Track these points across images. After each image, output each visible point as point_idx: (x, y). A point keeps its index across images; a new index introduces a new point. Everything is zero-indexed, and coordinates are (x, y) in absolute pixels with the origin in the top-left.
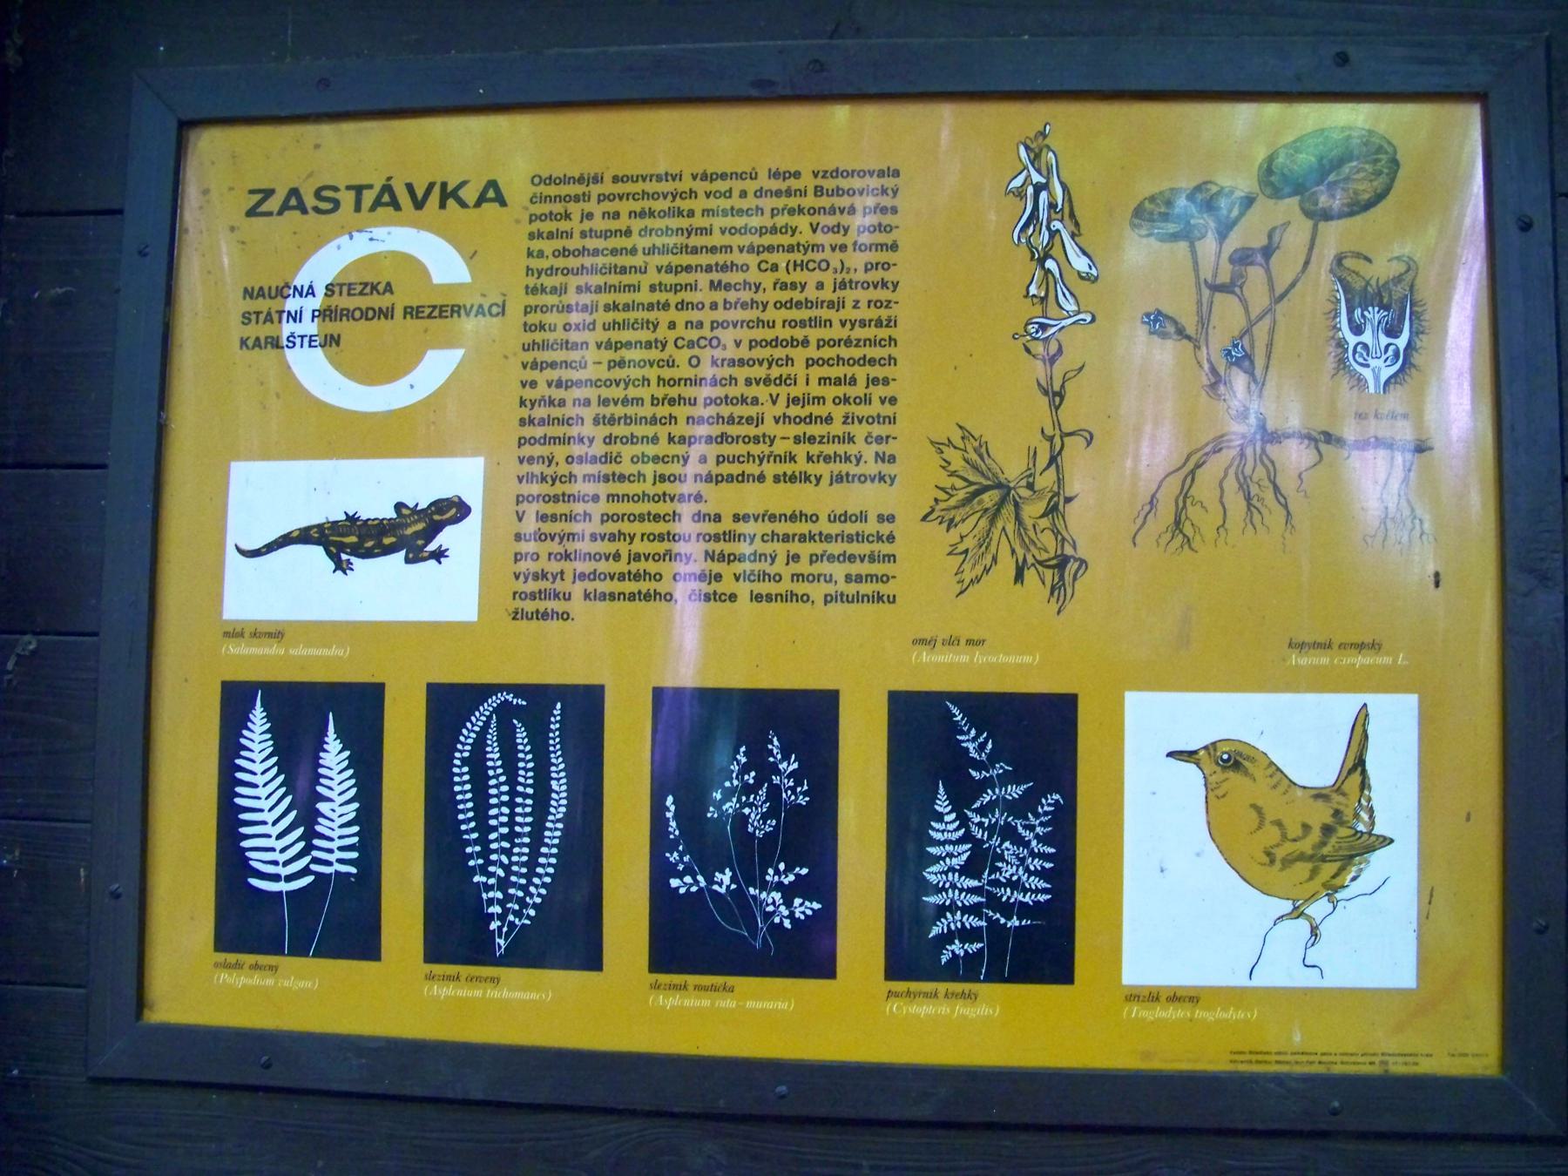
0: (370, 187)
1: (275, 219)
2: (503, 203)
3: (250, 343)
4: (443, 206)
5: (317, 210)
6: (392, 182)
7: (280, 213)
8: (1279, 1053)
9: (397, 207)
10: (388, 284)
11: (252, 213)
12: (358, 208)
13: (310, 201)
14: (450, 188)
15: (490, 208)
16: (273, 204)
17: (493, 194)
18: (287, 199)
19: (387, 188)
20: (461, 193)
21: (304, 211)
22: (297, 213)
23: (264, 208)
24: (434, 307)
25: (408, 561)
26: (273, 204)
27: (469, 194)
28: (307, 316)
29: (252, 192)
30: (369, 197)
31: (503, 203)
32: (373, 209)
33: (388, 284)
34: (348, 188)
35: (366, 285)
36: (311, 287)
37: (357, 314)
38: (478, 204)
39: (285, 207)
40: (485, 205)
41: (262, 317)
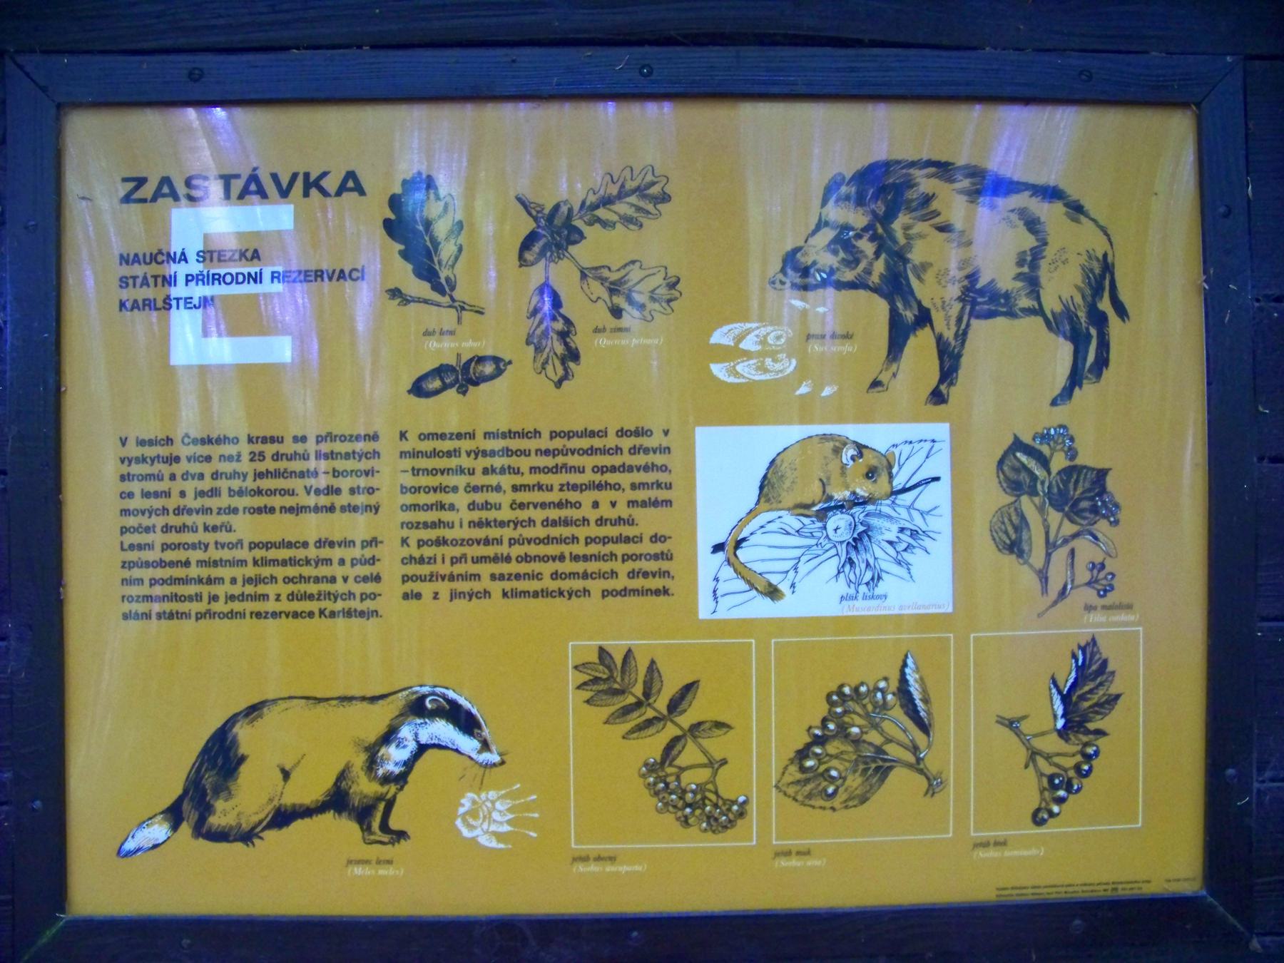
0: (237, 176)
2: (362, 192)
3: (128, 305)
4: (306, 194)
8: (1034, 887)
10: (256, 251)
11: (127, 199)
14: (312, 178)
16: (148, 190)
19: (253, 178)
20: (324, 183)
25: (401, 252)
27: (331, 184)
28: (181, 280)
29: (125, 180)
30: (237, 186)
31: (362, 192)
32: (241, 197)
33: (256, 251)
36: (183, 254)
37: (228, 279)
38: (339, 194)
39: (157, 195)
40: (345, 195)
41: (139, 281)
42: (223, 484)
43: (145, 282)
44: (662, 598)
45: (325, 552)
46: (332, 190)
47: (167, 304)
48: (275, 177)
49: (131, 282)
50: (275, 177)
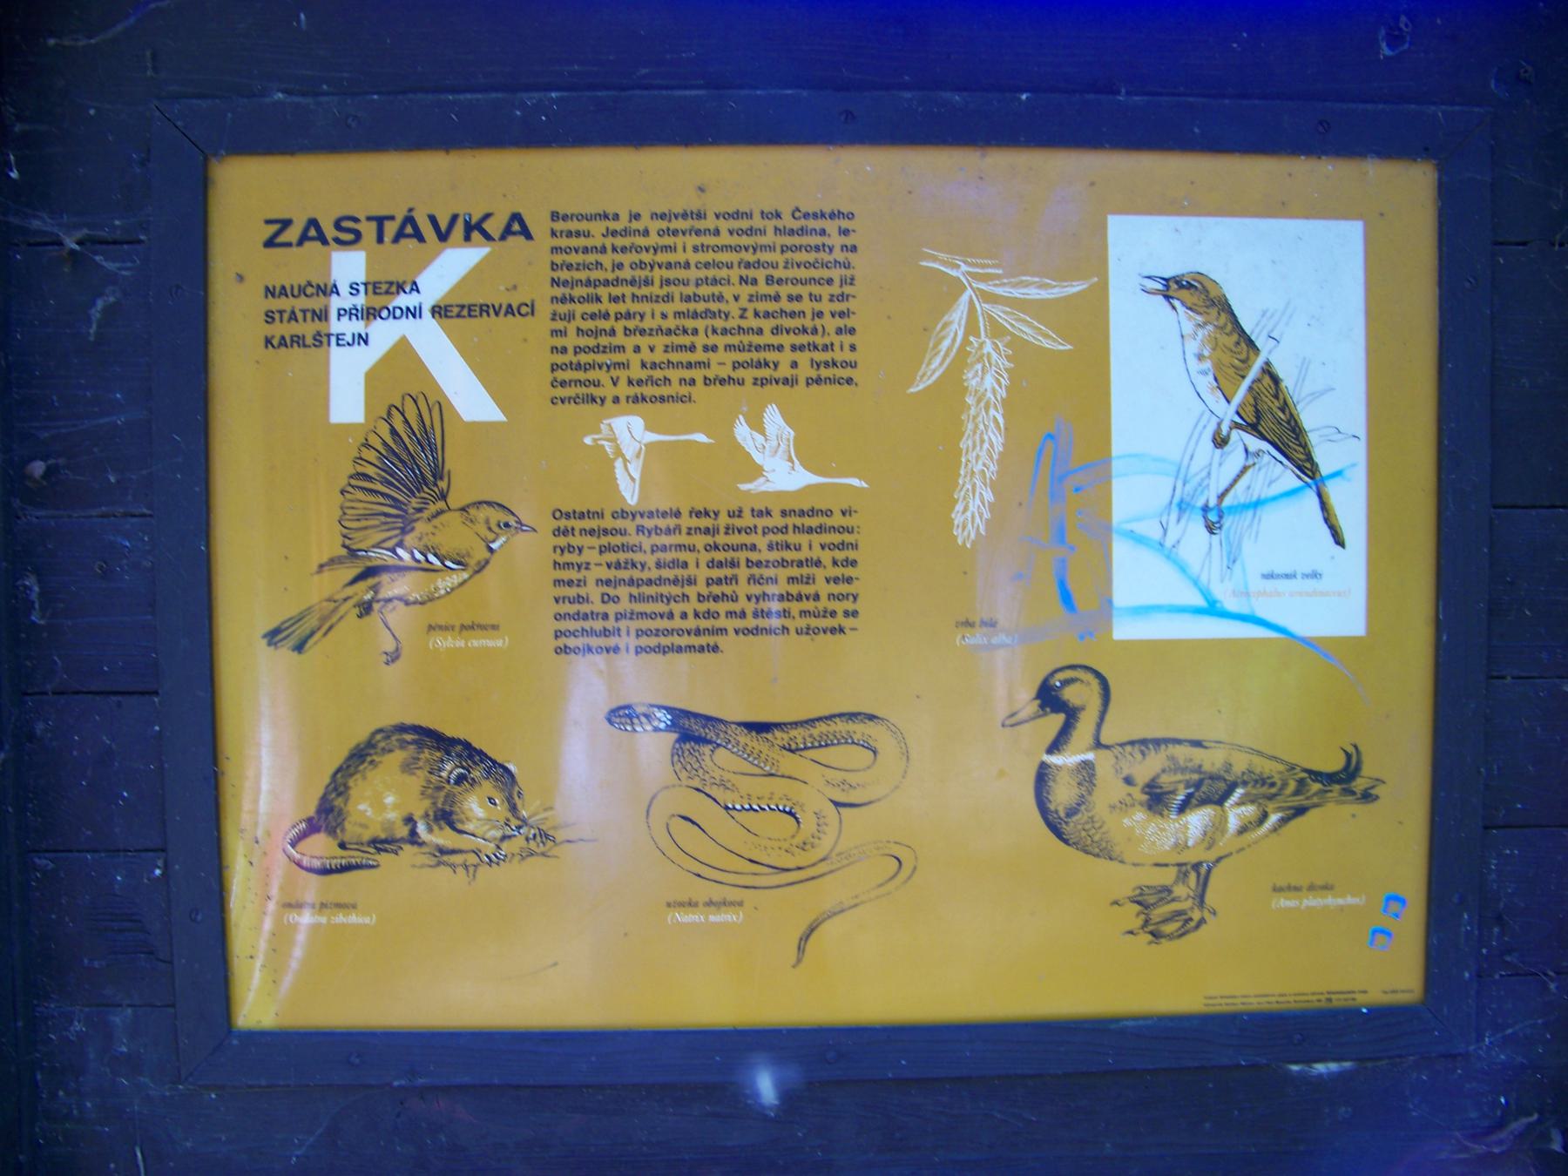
0: (392, 218)
1: (294, 249)
4: (467, 238)
5: (338, 241)
6: (414, 214)
7: (300, 243)
9: (421, 239)
11: (270, 243)
12: (380, 240)
13: (330, 232)
15: (516, 241)
16: (292, 234)
17: (517, 226)
18: (306, 230)
19: (409, 220)
20: (486, 226)
21: (325, 242)
22: (318, 244)
23: (281, 239)
24: (463, 307)
26: (292, 234)
27: (494, 227)
29: (268, 222)
30: (391, 229)
32: (396, 240)
34: (369, 219)
35: (391, 283)
38: (503, 238)
39: (304, 238)
41: (286, 316)
42: (676, 291)
43: (293, 317)
44: (838, 636)
45: (620, 524)
46: (496, 235)
47: (322, 339)
48: (433, 220)
49: (277, 316)
50: (433, 220)
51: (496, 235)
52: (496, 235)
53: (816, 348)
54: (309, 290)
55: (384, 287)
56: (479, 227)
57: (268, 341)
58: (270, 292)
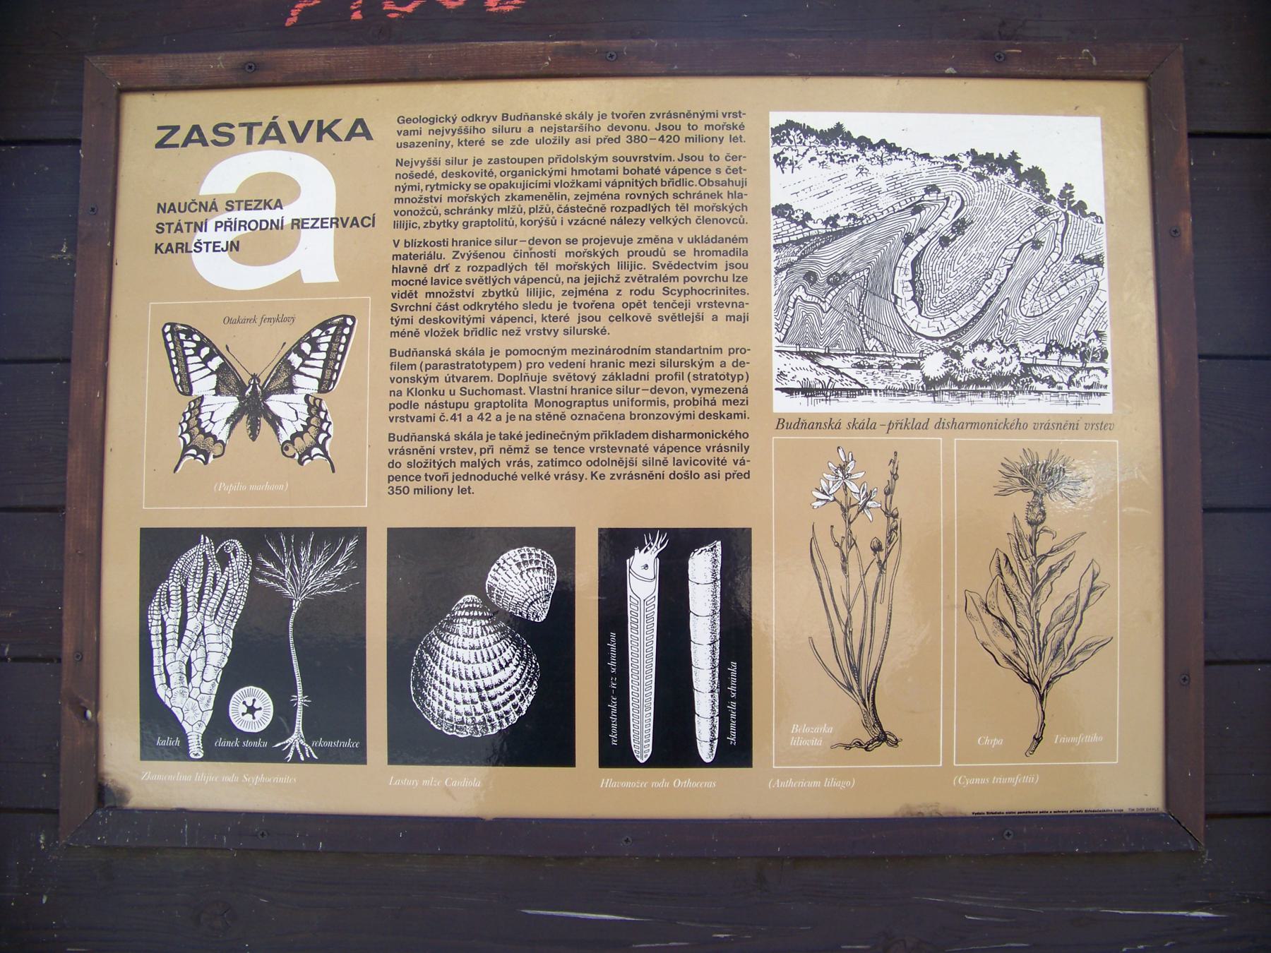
0: (260, 124)
3: (164, 248)
4: (319, 139)
5: (215, 143)
7: (185, 145)
9: (282, 141)
10: (279, 201)
11: (160, 145)
12: (249, 142)
13: (209, 136)
16: (179, 138)
18: (354, 127)
19: (273, 125)
21: (205, 144)
26: (179, 138)
27: (341, 130)
29: (160, 128)
30: (258, 133)
32: (262, 142)
33: (279, 201)
34: (242, 125)
36: (214, 203)
38: (348, 138)
39: (188, 140)
41: (173, 228)
46: (343, 136)
48: (292, 124)
49: (166, 227)
50: (292, 124)
51: (343, 137)
52: (343, 136)
53: (578, 184)
54: (193, 207)
55: (254, 204)
56: (329, 130)
57: (158, 248)
58: (161, 208)
